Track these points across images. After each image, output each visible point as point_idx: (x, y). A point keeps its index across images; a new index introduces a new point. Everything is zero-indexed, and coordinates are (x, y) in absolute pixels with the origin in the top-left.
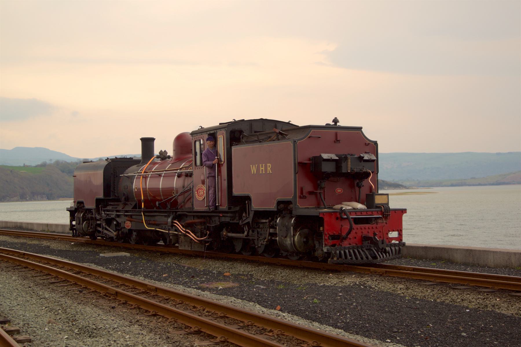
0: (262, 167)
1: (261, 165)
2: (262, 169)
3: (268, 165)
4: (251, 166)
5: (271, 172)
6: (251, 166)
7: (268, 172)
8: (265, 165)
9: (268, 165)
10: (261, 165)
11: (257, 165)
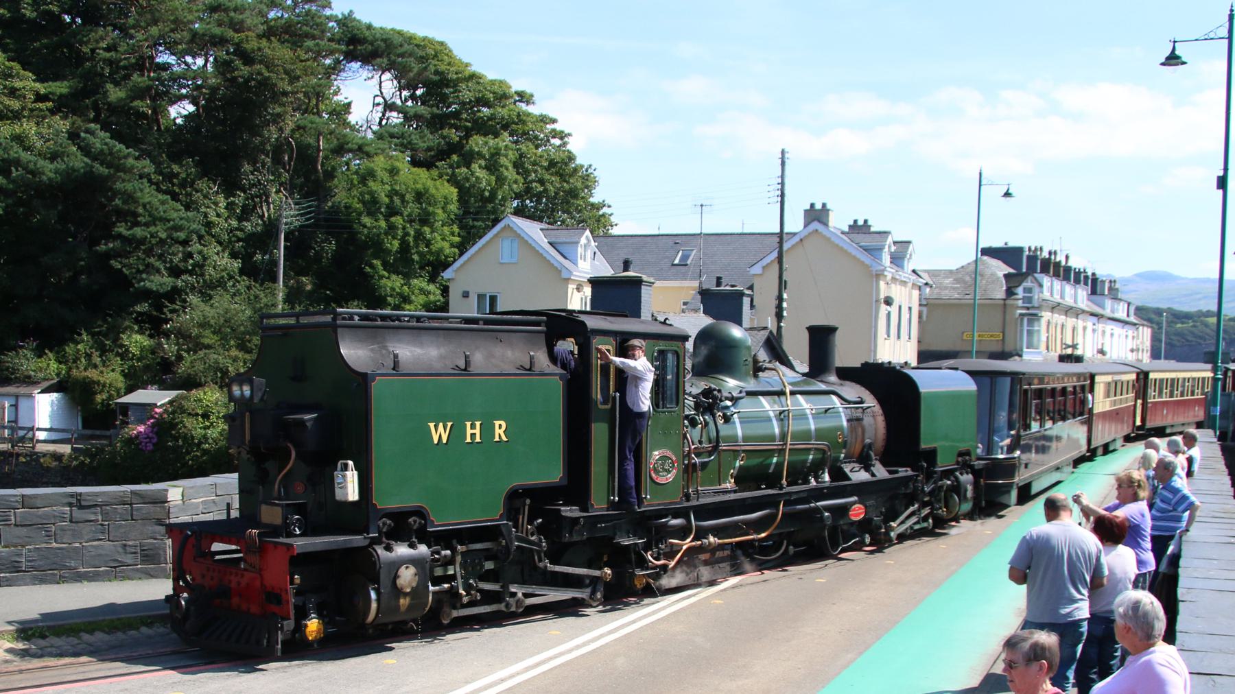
0: (473, 435)
1: (468, 424)
2: (473, 431)
3: (497, 423)
4: (432, 425)
5: (505, 439)
6: (432, 425)
7: (497, 439)
9: (497, 423)
10: (468, 424)
11: (449, 424)
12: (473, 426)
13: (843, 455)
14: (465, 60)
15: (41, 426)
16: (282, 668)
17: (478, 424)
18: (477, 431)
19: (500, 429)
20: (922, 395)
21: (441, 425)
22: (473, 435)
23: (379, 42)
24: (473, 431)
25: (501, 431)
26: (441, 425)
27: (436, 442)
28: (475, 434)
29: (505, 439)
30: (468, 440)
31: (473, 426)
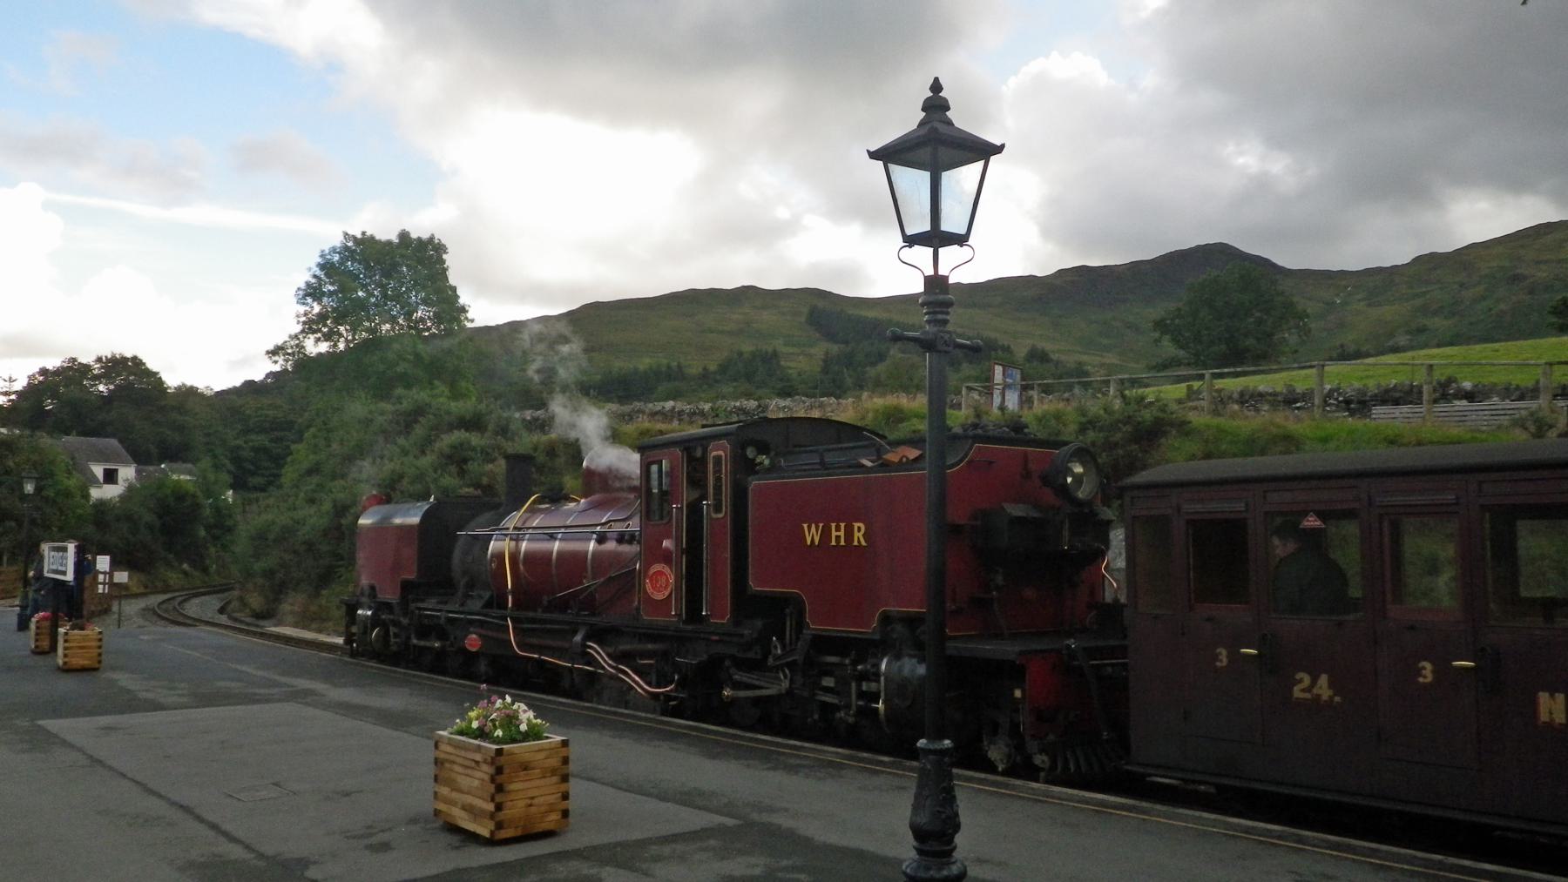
0: (838, 538)
1: (833, 525)
2: (838, 534)
3: (856, 525)
4: (805, 526)
5: (863, 543)
6: (805, 526)
7: (856, 543)
8: (845, 527)
9: (856, 525)
10: (833, 525)
11: (821, 525)
12: (838, 529)
13: (1349, 289)
14: (154, 370)
15: (123, 608)
16: (1525, 480)
17: (842, 525)
18: (834, 534)
19: (859, 536)
20: (132, 462)
21: (813, 526)
22: (838, 538)
23: (1089, 367)
24: (838, 534)
25: (860, 534)
26: (813, 526)
27: (809, 543)
28: (840, 536)
29: (863, 543)
30: (833, 543)
31: (838, 529)
